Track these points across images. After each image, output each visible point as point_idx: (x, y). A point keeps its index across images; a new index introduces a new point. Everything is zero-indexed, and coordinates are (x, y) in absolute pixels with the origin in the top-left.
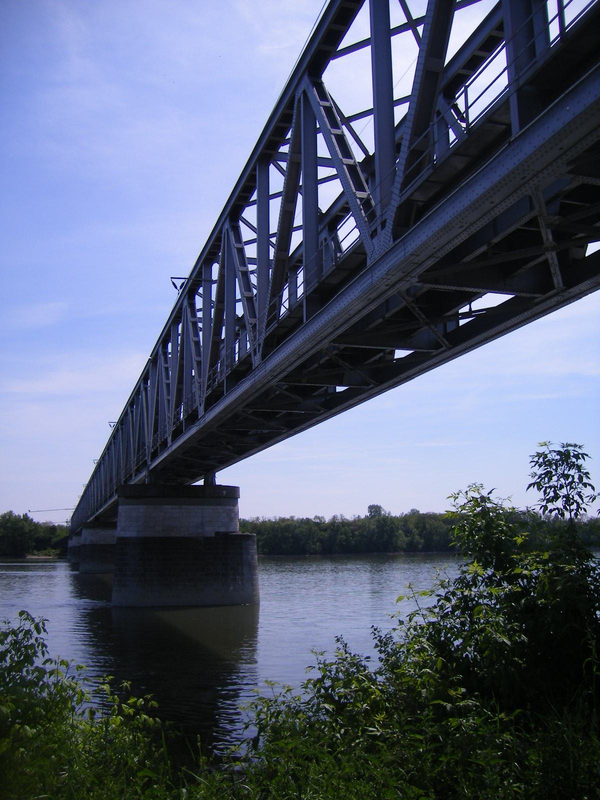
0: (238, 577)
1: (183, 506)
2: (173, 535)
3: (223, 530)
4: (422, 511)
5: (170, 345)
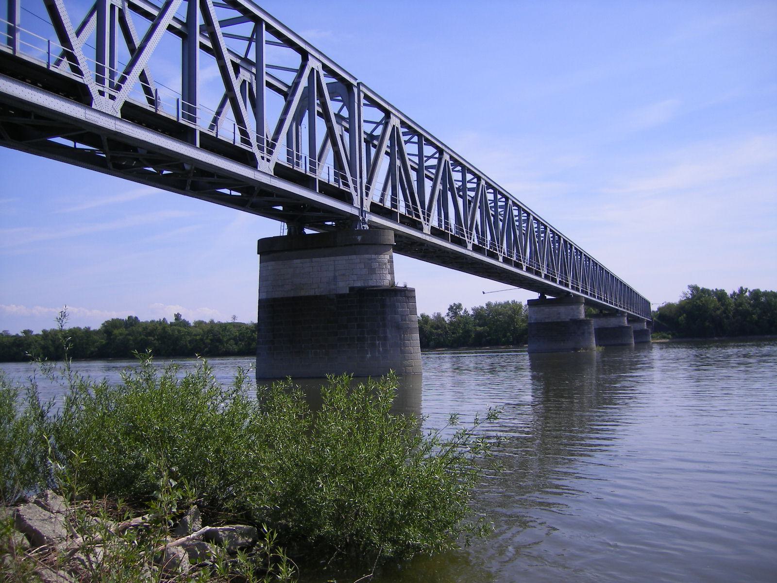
0: (378, 342)
3: (359, 284)
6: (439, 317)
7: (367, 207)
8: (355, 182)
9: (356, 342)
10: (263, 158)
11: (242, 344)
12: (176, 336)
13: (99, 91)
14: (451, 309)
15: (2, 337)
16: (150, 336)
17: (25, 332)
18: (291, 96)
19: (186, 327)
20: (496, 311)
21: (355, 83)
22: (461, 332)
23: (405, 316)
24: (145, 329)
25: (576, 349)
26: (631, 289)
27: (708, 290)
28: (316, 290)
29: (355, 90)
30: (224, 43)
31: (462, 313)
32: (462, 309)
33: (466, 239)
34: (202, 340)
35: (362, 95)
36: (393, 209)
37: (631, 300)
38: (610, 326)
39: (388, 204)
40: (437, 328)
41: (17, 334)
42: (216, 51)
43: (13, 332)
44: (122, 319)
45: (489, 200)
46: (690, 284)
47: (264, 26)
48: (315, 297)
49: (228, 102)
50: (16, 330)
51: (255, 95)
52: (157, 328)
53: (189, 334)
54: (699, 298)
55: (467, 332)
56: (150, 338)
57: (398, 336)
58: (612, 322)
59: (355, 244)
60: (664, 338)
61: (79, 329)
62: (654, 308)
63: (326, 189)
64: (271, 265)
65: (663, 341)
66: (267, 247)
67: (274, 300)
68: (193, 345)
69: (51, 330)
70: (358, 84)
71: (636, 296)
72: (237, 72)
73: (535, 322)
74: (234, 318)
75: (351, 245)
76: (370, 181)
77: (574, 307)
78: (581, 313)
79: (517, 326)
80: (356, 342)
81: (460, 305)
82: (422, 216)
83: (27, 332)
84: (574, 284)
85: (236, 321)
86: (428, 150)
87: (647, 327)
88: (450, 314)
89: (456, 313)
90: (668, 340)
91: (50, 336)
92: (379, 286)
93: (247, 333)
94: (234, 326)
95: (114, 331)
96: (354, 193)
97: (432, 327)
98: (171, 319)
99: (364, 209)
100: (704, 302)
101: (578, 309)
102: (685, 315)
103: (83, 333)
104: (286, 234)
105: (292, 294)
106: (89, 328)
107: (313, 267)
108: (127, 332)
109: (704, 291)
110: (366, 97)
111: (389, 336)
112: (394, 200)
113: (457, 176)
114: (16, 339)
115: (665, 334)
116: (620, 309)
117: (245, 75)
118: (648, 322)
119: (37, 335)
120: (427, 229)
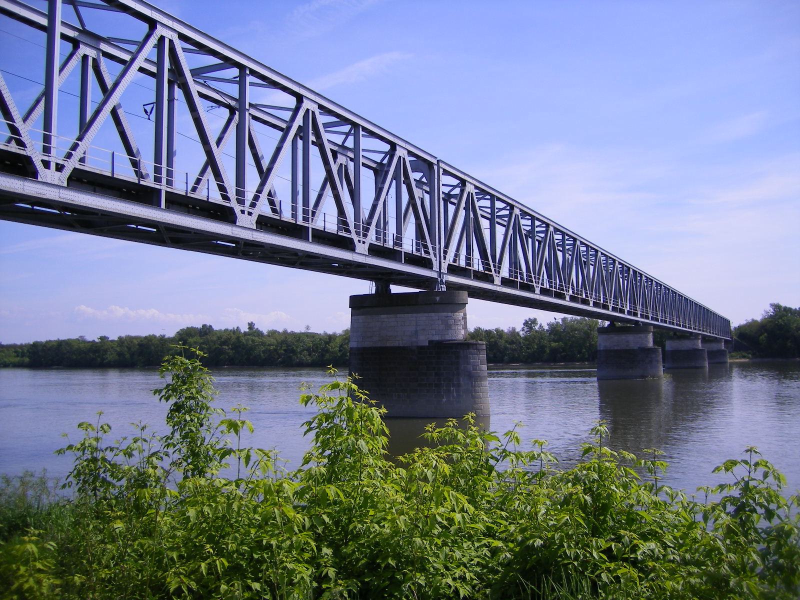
0: (452, 388)
1: (398, 315)
2: (388, 344)
3: (436, 338)
4: (61, 339)
5: (84, 180)
6: (513, 333)
7: (444, 269)
8: (434, 249)
9: (434, 388)
10: (359, 241)
11: (315, 355)
12: (250, 345)
13: (241, 210)
14: (526, 323)
15: (78, 342)
16: (224, 345)
17: (101, 338)
18: (382, 184)
19: (260, 337)
20: (572, 326)
21: (435, 162)
22: (536, 347)
23: (476, 366)
24: (219, 338)
25: (643, 377)
26: (708, 310)
27: (790, 309)
28: (400, 342)
29: (436, 167)
30: (326, 136)
31: (537, 328)
32: (537, 324)
33: (534, 284)
34: (275, 350)
35: (441, 171)
36: (467, 267)
37: (707, 322)
38: (683, 349)
39: (462, 263)
40: (512, 343)
41: (94, 341)
42: (320, 144)
43: (89, 338)
44: (197, 327)
45: (556, 239)
46: (772, 302)
47: (361, 129)
48: (399, 348)
49: (328, 185)
50: (92, 336)
51: (353, 185)
52: (231, 337)
53: (263, 344)
54: (781, 317)
55: (542, 348)
56: (225, 347)
57: (470, 383)
58: (686, 345)
59: (435, 304)
60: (744, 357)
61: (154, 336)
62: (734, 324)
63: (411, 259)
64: (361, 318)
65: (743, 360)
66: (357, 303)
67: (364, 348)
68: (266, 355)
69: (126, 337)
70: (438, 161)
71: (714, 316)
72: (335, 157)
73: (604, 349)
74: (308, 328)
75: (430, 304)
76: (447, 246)
77: (642, 335)
78: (649, 342)
79: (593, 343)
80: (434, 388)
81: (535, 319)
82: (493, 269)
83: (103, 338)
84: (643, 312)
85: (310, 331)
86: (499, 205)
87: (725, 347)
88: (525, 329)
89: (531, 328)
90: (747, 360)
91: (126, 342)
92: (455, 340)
93: (320, 344)
94: (307, 336)
95: (189, 339)
96: (433, 258)
97: (506, 342)
98: (244, 329)
99: (442, 271)
100: (786, 321)
101: (646, 337)
102: (766, 334)
103: (158, 341)
104: (374, 292)
105: (379, 345)
106: (164, 336)
107: (397, 322)
108: (202, 341)
109: (787, 310)
110: (444, 170)
111: (462, 382)
112: (468, 259)
113: (525, 223)
114: (92, 345)
115: (744, 354)
116: (694, 331)
117: (341, 159)
118: (726, 342)
119: (112, 341)
120: (497, 281)
